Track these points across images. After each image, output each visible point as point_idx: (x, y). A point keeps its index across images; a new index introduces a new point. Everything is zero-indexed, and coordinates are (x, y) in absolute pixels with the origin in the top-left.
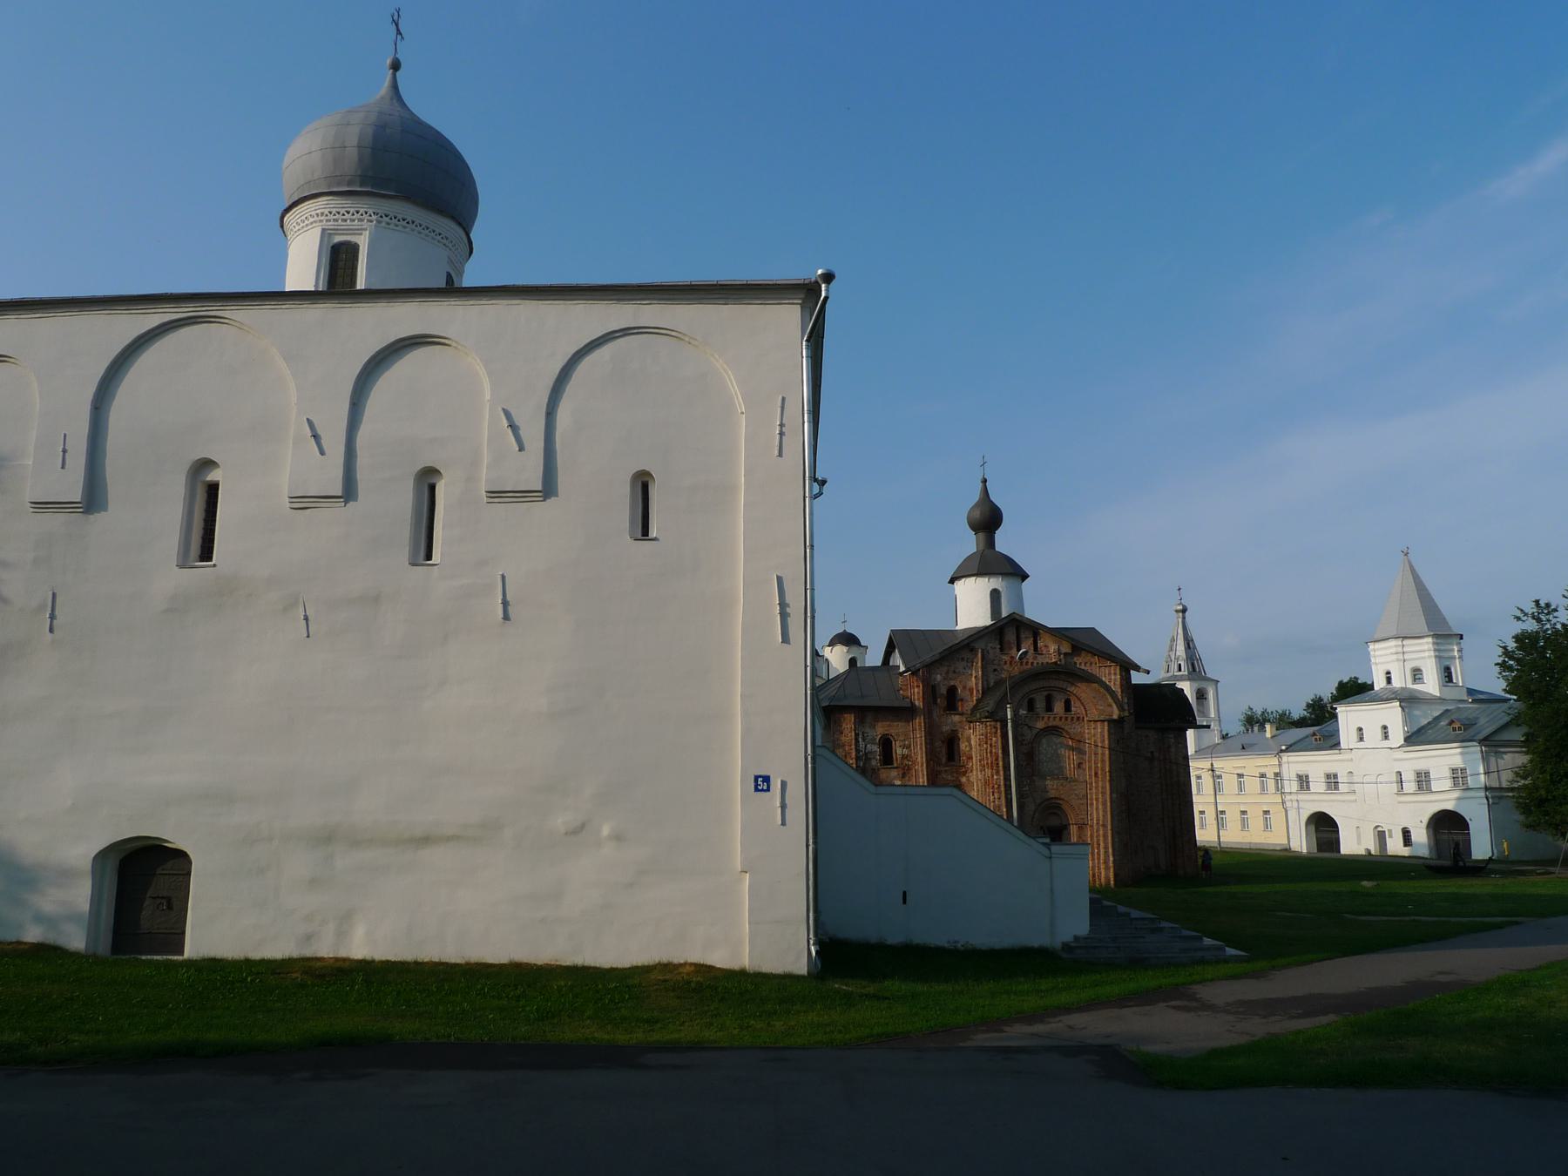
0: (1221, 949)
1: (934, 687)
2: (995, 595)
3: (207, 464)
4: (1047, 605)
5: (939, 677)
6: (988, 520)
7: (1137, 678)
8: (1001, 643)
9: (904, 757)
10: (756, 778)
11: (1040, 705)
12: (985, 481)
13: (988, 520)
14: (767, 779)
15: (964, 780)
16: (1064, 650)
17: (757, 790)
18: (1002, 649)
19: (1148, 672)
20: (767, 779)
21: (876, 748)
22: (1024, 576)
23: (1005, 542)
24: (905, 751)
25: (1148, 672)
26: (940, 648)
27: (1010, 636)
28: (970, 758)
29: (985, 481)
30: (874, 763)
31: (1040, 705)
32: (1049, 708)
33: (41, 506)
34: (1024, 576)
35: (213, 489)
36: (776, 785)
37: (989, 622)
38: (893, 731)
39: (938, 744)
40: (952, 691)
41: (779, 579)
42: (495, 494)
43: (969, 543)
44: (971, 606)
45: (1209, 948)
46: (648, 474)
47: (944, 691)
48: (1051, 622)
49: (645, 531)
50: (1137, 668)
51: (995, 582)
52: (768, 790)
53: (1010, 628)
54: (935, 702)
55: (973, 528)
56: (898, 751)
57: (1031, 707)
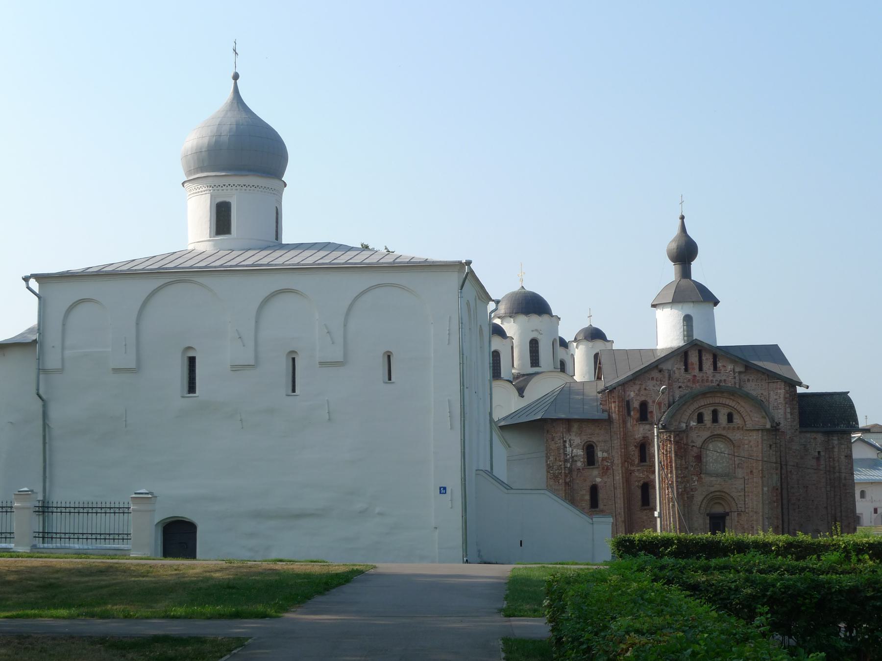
1: (628, 403)
4: (730, 330)
5: (632, 394)
6: (685, 253)
7: (800, 390)
8: (686, 364)
9: (604, 459)
11: (708, 418)
12: (682, 218)
13: (685, 253)
14: (445, 488)
16: (738, 369)
18: (686, 370)
19: (807, 387)
20: (445, 488)
21: (580, 452)
22: (716, 302)
23: (699, 271)
24: (605, 455)
27: (694, 358)
29: (682, 218)
30: (579, 464)
31: (708, 418)
32: (715, 420)
33: (116, 370)
34: (716, 302)
36: (449, 491)
37: (682, 344)
40: (644, 406)
41: (449, 401)
42: (322, 364)
43: (670, 272)
44: (666, 332)
47: (636, 404)
49: (390, 379)
50: (800, 384)
51: (689, 309)
53: (695, 352)
54: (629, 414)
55: (673, 261)
56: (600, 454)
57: (700, 419)
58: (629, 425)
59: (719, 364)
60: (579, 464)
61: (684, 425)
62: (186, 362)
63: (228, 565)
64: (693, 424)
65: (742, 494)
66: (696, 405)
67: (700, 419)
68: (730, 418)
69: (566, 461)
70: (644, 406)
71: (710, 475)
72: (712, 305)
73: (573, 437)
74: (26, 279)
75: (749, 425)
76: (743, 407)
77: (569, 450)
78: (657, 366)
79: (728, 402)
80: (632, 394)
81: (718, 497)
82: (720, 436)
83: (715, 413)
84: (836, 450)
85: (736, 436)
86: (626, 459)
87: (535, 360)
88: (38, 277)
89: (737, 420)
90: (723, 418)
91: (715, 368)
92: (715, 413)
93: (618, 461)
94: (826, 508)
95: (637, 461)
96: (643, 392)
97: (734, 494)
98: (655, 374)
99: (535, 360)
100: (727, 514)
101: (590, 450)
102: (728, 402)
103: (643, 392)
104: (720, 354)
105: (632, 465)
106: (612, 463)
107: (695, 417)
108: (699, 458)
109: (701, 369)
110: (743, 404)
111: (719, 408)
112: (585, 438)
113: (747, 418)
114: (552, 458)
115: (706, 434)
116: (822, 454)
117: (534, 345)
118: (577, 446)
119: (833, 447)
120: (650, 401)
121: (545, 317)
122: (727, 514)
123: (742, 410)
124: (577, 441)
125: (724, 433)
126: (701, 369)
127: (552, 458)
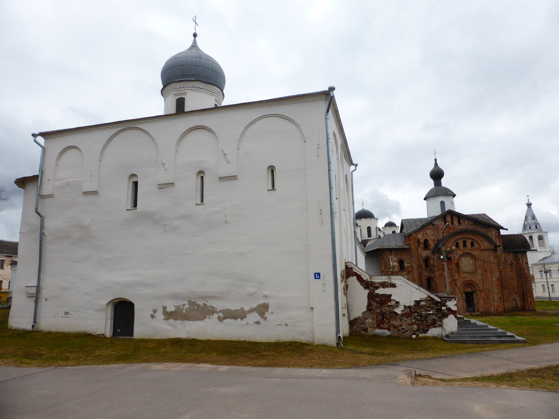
0: (497, 330)
1: (418, 240)
2: (442, 203)
3: (134, 175)
4: (465, 204)
5: (420, 236)
6: (437, 175)
7: (503, 232)
9: (408, 267)
10: (315, 274)
11: (461, 245)
12: (436, 160)
13: (437, 175)
14: (319, 274)
15: (404, 273)
17: (315, 278)
19: (507, 230)
20: (319, 274)
22: (454, 196)
23: (445, 182)
25: (507, 230)
26: (420, 225)
27: (449, 218)
28: (434, 266)
29: (436, 160)
30: (396, 269)
31: (461, 245)
34: (454, 196)
35: (136, 184)
38: (403, 258)
39: (421, 262)
40: (426, 241)
43: (431, 184)
45: (491, 330)
46: (273, 167)
47: (422, 241)
48: (465, 213)
50: (503, 228)
52: (320, 278)
54: (419, 245)
57: (457, 245)
58: (419, 251)
59: (461, 221)
60: (396, 269)
61: (449, 249)
62: (131, 184)
63: (22, 361)
64: (454, 248)
65: (481, 281)
66: (455, 239)
67: (457, 245)
68: (472, 245)
69: (390, 268)
70: (426, 241)
71: (464, 273)
72: (451, 198)
73: (393, 257)
74: (34, 135)
75: (483, 248)
76: (479, 239)
77: (391, 263)
78: (431, 223)
79: (471, 236)
80: (420, 236)
81: (470, 284)
82: (468, 253)
83: (465, 243)
84: (521, 260)
85: (476, 253)
86: (419, 266)
87: (369, 235)
88: (43, 134)
89: (476, 245)
90: (469, 245)
91: (459, 223)
92: (465, 243)
93: (415, 267)
94: (518, 288)
95: (424, 268)
96: (425, 235)
97: (477, 282)
98: (431, 227)
99: (369, 235)
100: (474, 292)
101: (401, 263)
102: (471, 236)
103: (425, 235)
104: (460, 217)
105: (422, 269)
106: (412, 269)
107: (455, 244)
108: (458, 265)
109: (452, 224)
110: (479, 237)
111: (467, 240)
112: (399, 257)
113: (481, 244)
114: (383, 267)
115: (461, 253)
116: (514, 262)
117: (369, 229)
118: (395, 261)
119: (519, 259)
120: (429, 239)
121: (373, 219)
122: (474, 292)
123: (478, 240)
124: (395, 259)
125: (470, 252)
126: (452, 224)
127: (383, 267)
